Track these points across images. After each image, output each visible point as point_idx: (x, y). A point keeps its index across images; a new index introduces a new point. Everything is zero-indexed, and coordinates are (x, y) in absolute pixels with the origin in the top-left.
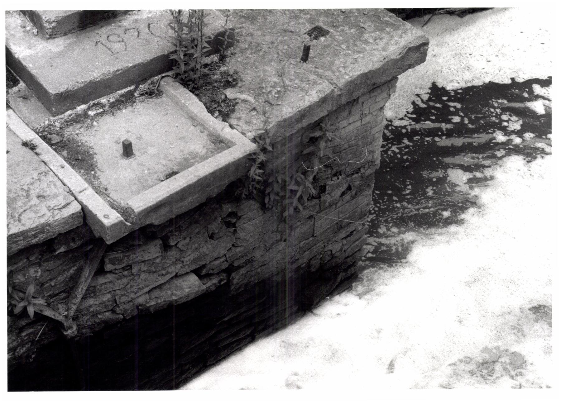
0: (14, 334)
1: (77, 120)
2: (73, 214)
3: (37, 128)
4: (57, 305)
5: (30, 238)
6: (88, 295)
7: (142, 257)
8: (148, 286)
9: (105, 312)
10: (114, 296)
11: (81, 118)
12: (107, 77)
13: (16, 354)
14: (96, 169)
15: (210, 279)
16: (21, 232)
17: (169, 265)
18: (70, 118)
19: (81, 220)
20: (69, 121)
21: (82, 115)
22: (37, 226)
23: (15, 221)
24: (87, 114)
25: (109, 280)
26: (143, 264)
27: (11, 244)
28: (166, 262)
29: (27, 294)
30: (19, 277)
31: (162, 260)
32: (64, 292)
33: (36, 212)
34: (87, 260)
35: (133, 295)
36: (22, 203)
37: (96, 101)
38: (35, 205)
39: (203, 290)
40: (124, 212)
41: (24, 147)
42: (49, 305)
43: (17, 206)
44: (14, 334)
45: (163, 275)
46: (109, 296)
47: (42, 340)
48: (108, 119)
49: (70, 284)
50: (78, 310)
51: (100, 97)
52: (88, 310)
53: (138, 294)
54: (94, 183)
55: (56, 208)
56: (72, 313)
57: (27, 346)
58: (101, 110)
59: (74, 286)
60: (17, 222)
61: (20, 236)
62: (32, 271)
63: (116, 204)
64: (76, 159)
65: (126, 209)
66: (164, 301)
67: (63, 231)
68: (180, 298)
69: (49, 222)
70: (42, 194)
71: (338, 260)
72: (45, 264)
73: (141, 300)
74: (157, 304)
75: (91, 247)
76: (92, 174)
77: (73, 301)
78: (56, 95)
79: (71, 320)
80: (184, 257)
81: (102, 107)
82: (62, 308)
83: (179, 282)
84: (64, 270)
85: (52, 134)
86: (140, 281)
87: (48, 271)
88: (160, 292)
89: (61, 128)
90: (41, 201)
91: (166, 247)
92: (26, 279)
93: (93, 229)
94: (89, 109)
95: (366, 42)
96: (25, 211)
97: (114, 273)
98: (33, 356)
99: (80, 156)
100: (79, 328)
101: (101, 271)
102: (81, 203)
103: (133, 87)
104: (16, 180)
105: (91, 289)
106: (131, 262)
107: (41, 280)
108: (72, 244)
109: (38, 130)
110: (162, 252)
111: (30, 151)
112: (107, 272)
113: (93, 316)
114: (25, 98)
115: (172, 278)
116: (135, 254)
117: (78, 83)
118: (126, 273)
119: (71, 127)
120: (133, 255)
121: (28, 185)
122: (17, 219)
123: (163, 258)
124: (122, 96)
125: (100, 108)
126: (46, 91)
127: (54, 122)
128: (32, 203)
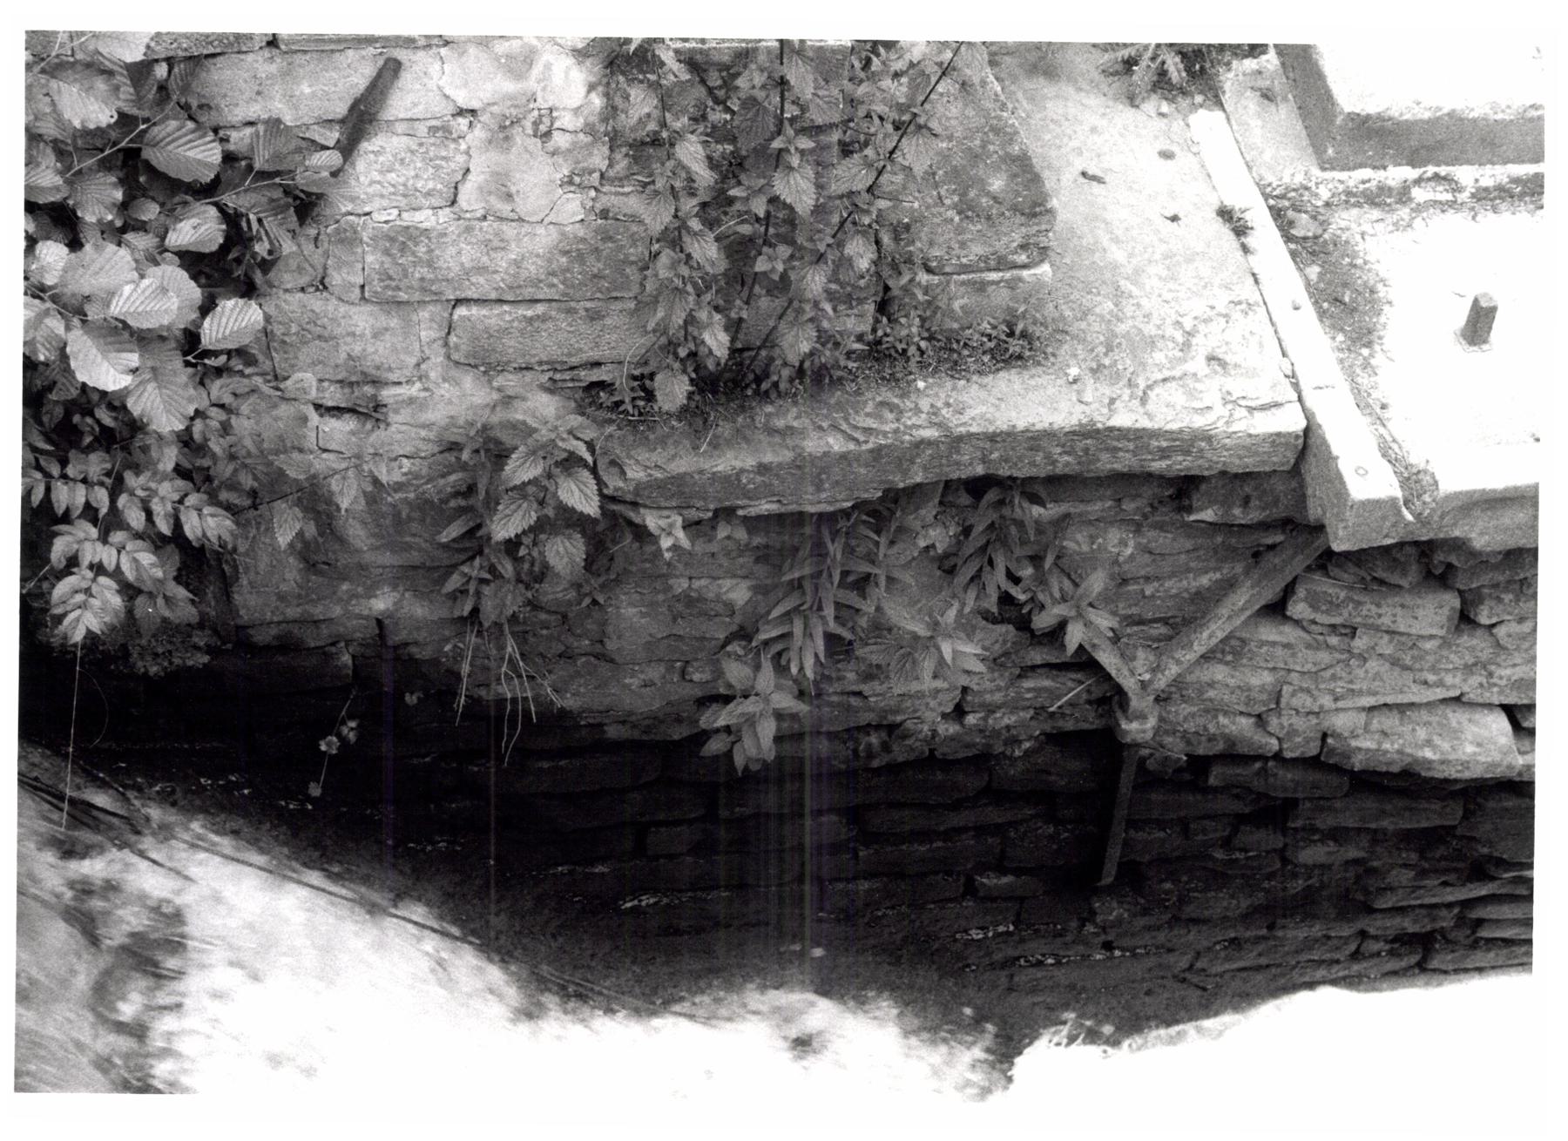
0: (1007, 674)
1: (1375, 198)
2: (1279, 434)
3: (1270, 185)
4: (1135, 647)
5: (1150, 453)
6: (1219, 655)
7: (1394, 622)
8: (1375, 694)
9: (1241, 713)
10: (1282, 683)
11: (1389, 197)
12: (1500, 116)
13: (990, 721)
14: (1377, 347)
16: (1137, 430)
17: (1451, 666)
18: (1362, 187)
19: (1291, 457)
20: (1355, 195)
21: (1395, 193)
22: (1181, 431)
23: (1132, 397)
24: (1409, 192)
25: (1285, 641)
26: (1386, 638)
27: (1101, 450)
28: (1447, 658)
29: (1080, 591)
30: (1079, 537)
31: (1440, 647)
32: (1165, 621)
33: (1191, 394)
34: (156, 965)
35: (1327, 701)
36: (1166, 356)
37: (1443, 170)
38: (1195, 375)
39: (1510, 767)
40: (1409, 479)
41: (1220, 219)
42: (1116, 639)
43: (1150, 361)
44: (1007, 674)
45: (1425, 683)
46: (1267, 678)
47: (1063, 715)
48: (1456, 221)
49: (1189, 610)
50: (1178, 682)
51: (1455, 161)
52: (1201, 692)
53: (1340, 704)
54: (1359, 380)
55: (1243, 403)
56: (1161, 682)
57: (1021, 714)
58: (1449, 197)
59: (1196, 619)
60: (1136, 402)
61: (1129, 440)
62: (1114, 536)
63: (1397, 450)
64: (1336, 300)
65: (1419, 472)
66: (1400, 752)
67: (1236, 466)
68: (1443, 762)
69: (1213, 432)
70: (1221, 356)
72: (1152, 534)
73: (1341, 722)
74: (1378, 750)
75: (1279, 538)
76: (1360, 354)
77: (1178, 655)
78: (1352, 117)
79: (1152, 698)
80: (1499, 665)
81: (1454, 190)
82: (1143, 658)
83: (1456, 717)
84: (1189, 570)
85: (1300, 211)
86: (1361, 673)
87: (1150, 553)
88: (1397, 722)
89: (1327, 204)
90: (1216, 372)
91: (1465, 619)
92: (1093, 551)
93: (1309, 492)
94: (1418, 182)
96: (1165, 380)
97: (1304, 628)
98: (1027, 745)
99: (1348, 293)
100: (1159, 727)
101: (1276, 609)
102: (1309, 416)
104: (1168, 296)
105: (1234, 642)
106: (1359, 620)
107: (1126, 567)
108: (1237, 511)
109: (1269, 190)
110: (1449, 629)
111: (1232, 236)
112: (1287, 619)
113: (1207, 711)
114: (1267, 96)
115: (1444, 701)
116: (1378, 605)
117: (1418, 104)
118: (1334, 640)
119: (1355, 211)
120: (1373, 607)
121: (1196, 318)
122: (1141, 394)
123: (1445, 643)
124: (1516, 181)
125: (1447, 191)
126: (1328, 97)
127: (1317, 184)
128: (1190, 367)
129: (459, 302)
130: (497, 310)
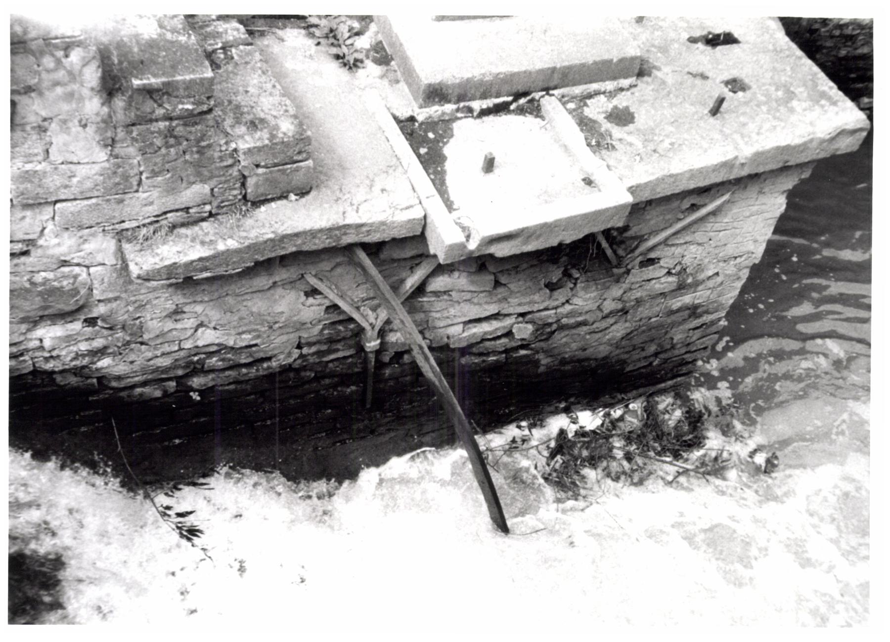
15: (404, 424)
71: (744, 479)
95: (792, 110)
103: (510, 99)
129: (56, 202)
130: (75, 203)
